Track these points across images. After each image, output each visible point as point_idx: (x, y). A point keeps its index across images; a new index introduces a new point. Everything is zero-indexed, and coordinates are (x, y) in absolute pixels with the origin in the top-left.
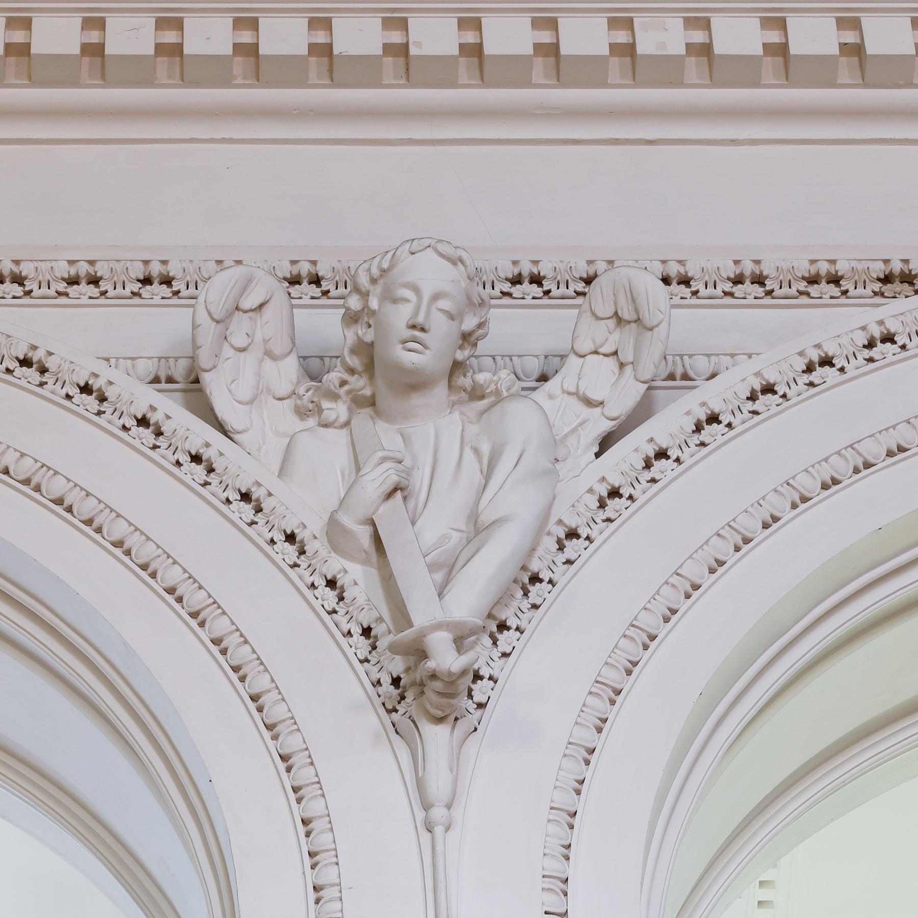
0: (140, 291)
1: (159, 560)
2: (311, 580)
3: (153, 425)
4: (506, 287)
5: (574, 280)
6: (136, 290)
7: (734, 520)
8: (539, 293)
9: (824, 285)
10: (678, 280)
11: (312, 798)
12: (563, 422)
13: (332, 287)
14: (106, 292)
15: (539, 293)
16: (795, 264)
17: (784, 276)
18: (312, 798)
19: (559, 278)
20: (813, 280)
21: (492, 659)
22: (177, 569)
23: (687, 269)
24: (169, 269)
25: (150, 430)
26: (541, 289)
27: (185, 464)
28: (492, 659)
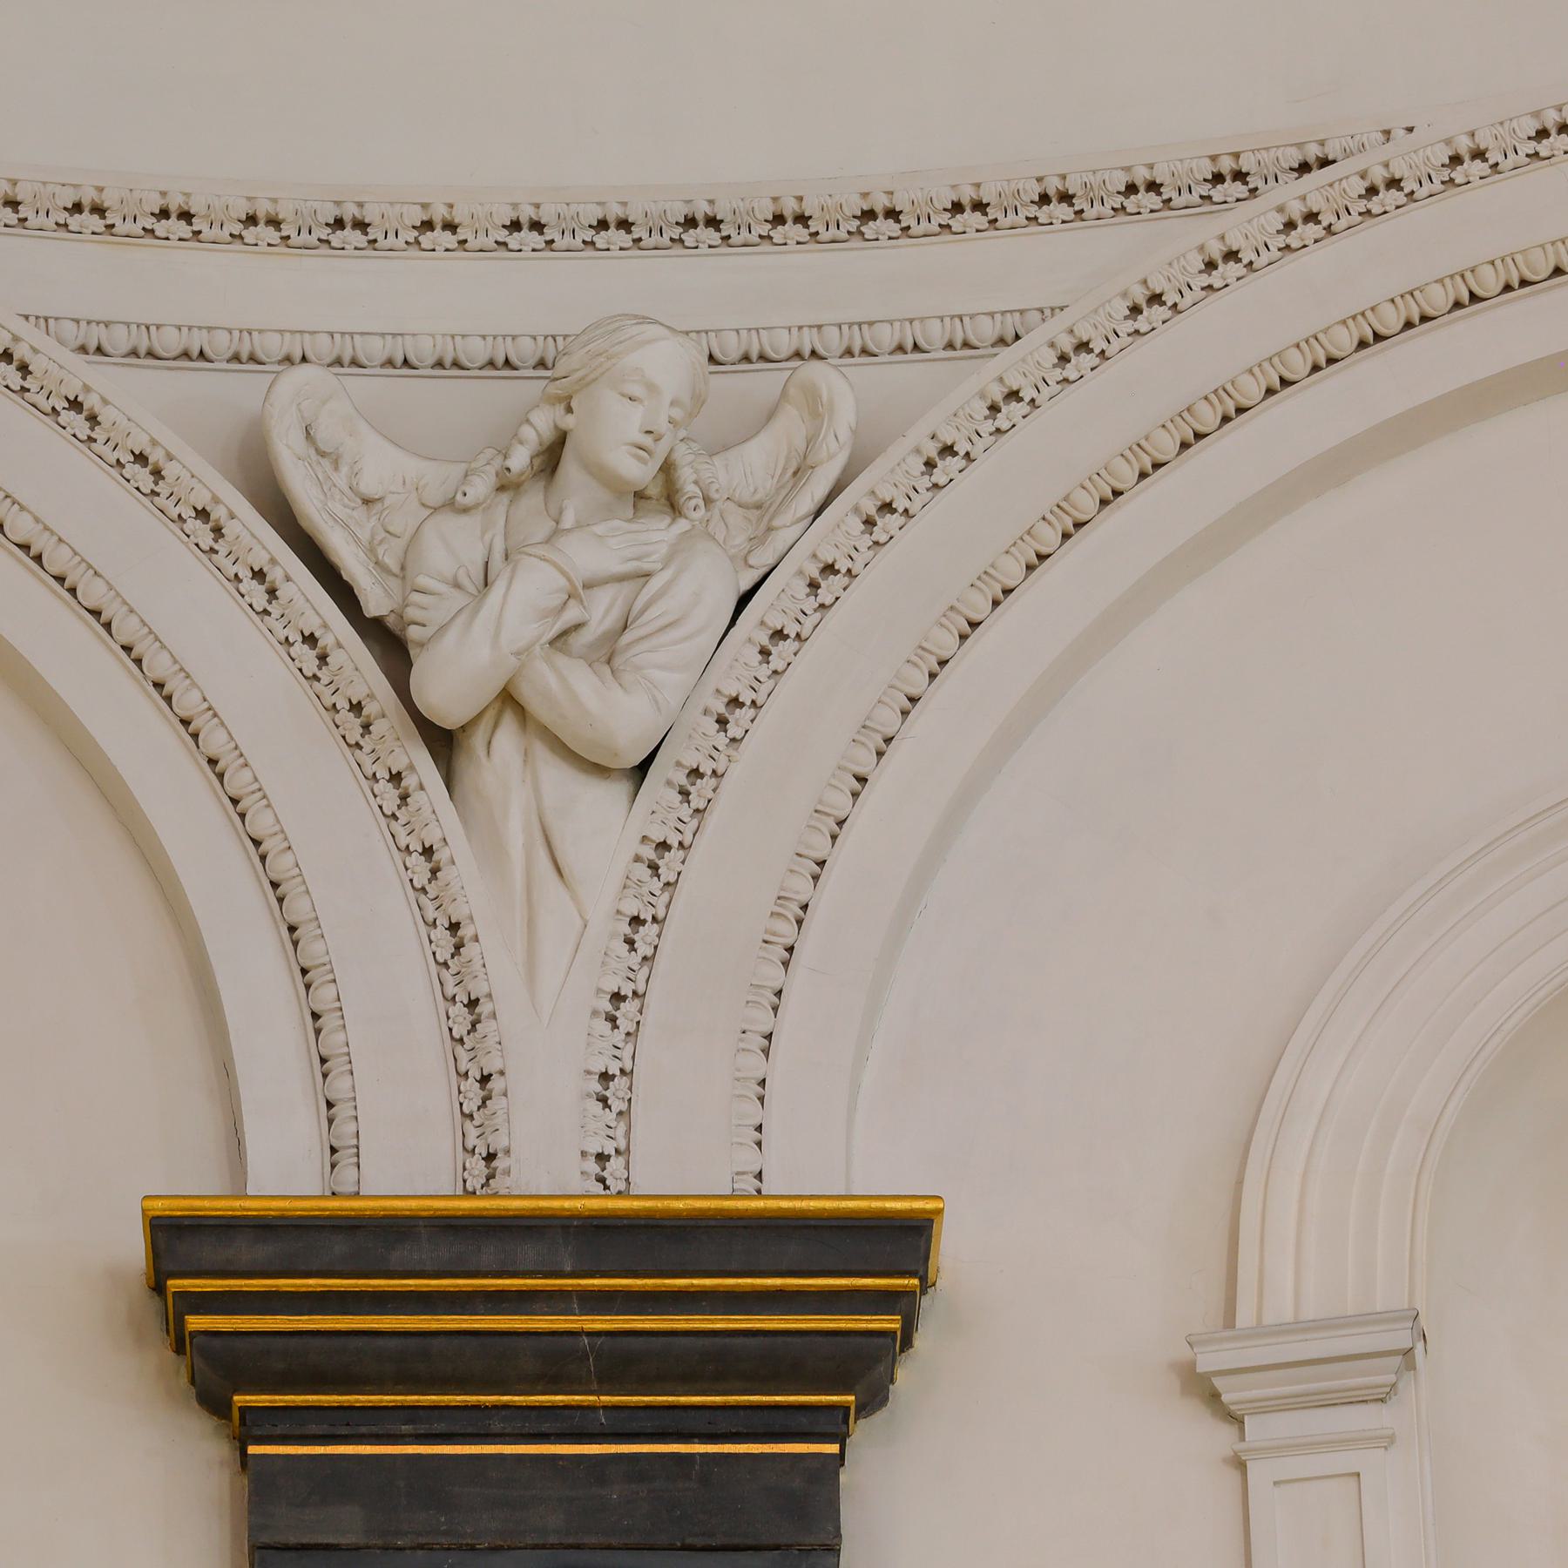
1: (294, 881)
2: (407, 842)
3: (364, 716)
4: (149, 223)
5: (495, 229)
6: (588, 239)
7: (158, 327)
8: (983, 224)
9: (525, 232)
11: (323, 984)
12: (664, 541)
13: (1500, 159)
14: (26, 219)
15: (983, 224)
16: (667, 206)
17: (303, 222)
18: (323, 984)
19: (213, 216)
20: (868, 215)
21: (681, 821)
22: (270, 819)
23: (364, 214)
24: (103, 197)
25: (359, 721)
26: (1072, 209)
27: (245, 580)
28: (681, 821)
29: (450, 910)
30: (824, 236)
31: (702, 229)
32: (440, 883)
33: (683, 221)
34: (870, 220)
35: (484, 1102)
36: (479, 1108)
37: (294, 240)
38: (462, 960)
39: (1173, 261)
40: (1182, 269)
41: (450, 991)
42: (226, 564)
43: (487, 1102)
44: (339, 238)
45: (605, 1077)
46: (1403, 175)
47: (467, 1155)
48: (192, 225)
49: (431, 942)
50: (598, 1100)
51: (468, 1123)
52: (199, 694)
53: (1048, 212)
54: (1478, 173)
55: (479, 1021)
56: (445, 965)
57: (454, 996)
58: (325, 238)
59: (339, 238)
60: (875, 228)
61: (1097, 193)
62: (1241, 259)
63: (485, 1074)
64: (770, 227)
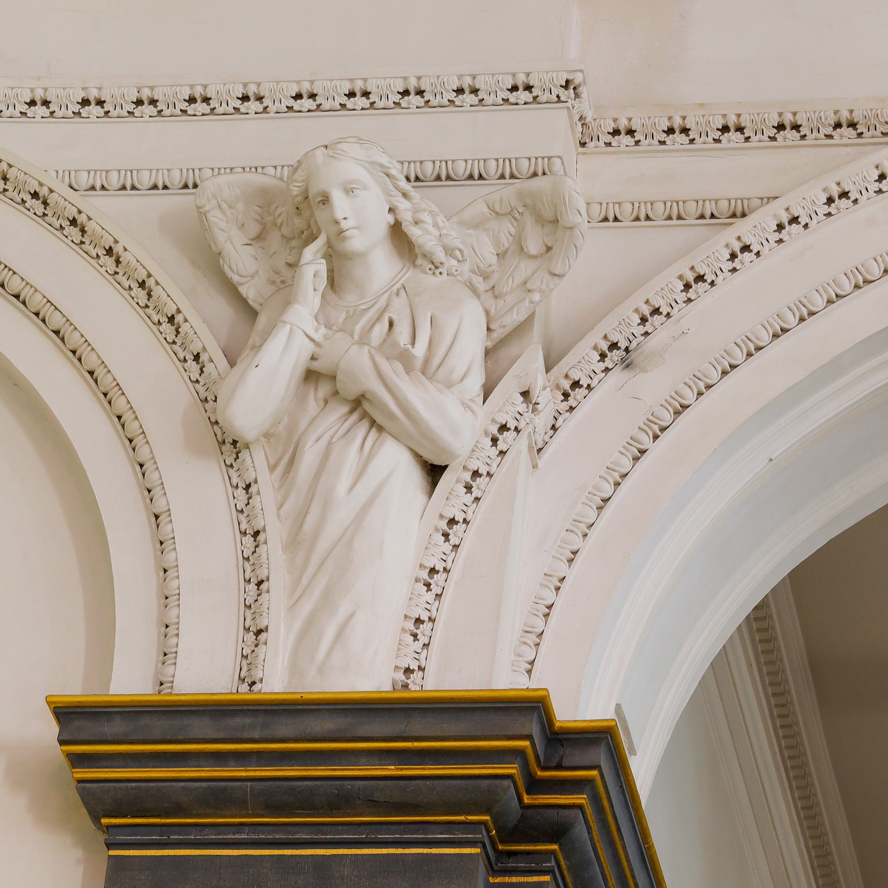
0: (776, 136)
10: (847, 124)
11: (170, 665)
29: (191, 348)
30: (220, 110)
31: (305, 100)
32: (182, 334)
33: (188, 99)
34: (32, 106)
35: (237, 456)
36: (200, 375)
37: (434, 102)
38: (206, 375)
39: (874, 109)
40: (876, 115)
41: (235, 481)
42: (54, 221)
43: (203, 369)
44: (460, 99)
45: (418, 621)
46: (318, 92)
47: (204, 403)
48: (104, 108)
49: (234, 498)
50: (411, 635)
51: (230, 470)
52: (41, 295)
53: (408, 100)
54: (96, 114)
55: (204, 366)
56: (197, 381)
57: (206, 398)
58: (397, 101)
59: (86, 111)
60: (783, 135)
61: (225, 97)
62: (157, 106)
63: (195, 354)
64: (401, 97)
